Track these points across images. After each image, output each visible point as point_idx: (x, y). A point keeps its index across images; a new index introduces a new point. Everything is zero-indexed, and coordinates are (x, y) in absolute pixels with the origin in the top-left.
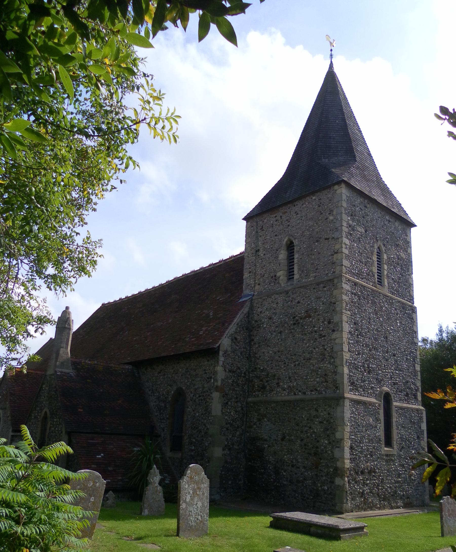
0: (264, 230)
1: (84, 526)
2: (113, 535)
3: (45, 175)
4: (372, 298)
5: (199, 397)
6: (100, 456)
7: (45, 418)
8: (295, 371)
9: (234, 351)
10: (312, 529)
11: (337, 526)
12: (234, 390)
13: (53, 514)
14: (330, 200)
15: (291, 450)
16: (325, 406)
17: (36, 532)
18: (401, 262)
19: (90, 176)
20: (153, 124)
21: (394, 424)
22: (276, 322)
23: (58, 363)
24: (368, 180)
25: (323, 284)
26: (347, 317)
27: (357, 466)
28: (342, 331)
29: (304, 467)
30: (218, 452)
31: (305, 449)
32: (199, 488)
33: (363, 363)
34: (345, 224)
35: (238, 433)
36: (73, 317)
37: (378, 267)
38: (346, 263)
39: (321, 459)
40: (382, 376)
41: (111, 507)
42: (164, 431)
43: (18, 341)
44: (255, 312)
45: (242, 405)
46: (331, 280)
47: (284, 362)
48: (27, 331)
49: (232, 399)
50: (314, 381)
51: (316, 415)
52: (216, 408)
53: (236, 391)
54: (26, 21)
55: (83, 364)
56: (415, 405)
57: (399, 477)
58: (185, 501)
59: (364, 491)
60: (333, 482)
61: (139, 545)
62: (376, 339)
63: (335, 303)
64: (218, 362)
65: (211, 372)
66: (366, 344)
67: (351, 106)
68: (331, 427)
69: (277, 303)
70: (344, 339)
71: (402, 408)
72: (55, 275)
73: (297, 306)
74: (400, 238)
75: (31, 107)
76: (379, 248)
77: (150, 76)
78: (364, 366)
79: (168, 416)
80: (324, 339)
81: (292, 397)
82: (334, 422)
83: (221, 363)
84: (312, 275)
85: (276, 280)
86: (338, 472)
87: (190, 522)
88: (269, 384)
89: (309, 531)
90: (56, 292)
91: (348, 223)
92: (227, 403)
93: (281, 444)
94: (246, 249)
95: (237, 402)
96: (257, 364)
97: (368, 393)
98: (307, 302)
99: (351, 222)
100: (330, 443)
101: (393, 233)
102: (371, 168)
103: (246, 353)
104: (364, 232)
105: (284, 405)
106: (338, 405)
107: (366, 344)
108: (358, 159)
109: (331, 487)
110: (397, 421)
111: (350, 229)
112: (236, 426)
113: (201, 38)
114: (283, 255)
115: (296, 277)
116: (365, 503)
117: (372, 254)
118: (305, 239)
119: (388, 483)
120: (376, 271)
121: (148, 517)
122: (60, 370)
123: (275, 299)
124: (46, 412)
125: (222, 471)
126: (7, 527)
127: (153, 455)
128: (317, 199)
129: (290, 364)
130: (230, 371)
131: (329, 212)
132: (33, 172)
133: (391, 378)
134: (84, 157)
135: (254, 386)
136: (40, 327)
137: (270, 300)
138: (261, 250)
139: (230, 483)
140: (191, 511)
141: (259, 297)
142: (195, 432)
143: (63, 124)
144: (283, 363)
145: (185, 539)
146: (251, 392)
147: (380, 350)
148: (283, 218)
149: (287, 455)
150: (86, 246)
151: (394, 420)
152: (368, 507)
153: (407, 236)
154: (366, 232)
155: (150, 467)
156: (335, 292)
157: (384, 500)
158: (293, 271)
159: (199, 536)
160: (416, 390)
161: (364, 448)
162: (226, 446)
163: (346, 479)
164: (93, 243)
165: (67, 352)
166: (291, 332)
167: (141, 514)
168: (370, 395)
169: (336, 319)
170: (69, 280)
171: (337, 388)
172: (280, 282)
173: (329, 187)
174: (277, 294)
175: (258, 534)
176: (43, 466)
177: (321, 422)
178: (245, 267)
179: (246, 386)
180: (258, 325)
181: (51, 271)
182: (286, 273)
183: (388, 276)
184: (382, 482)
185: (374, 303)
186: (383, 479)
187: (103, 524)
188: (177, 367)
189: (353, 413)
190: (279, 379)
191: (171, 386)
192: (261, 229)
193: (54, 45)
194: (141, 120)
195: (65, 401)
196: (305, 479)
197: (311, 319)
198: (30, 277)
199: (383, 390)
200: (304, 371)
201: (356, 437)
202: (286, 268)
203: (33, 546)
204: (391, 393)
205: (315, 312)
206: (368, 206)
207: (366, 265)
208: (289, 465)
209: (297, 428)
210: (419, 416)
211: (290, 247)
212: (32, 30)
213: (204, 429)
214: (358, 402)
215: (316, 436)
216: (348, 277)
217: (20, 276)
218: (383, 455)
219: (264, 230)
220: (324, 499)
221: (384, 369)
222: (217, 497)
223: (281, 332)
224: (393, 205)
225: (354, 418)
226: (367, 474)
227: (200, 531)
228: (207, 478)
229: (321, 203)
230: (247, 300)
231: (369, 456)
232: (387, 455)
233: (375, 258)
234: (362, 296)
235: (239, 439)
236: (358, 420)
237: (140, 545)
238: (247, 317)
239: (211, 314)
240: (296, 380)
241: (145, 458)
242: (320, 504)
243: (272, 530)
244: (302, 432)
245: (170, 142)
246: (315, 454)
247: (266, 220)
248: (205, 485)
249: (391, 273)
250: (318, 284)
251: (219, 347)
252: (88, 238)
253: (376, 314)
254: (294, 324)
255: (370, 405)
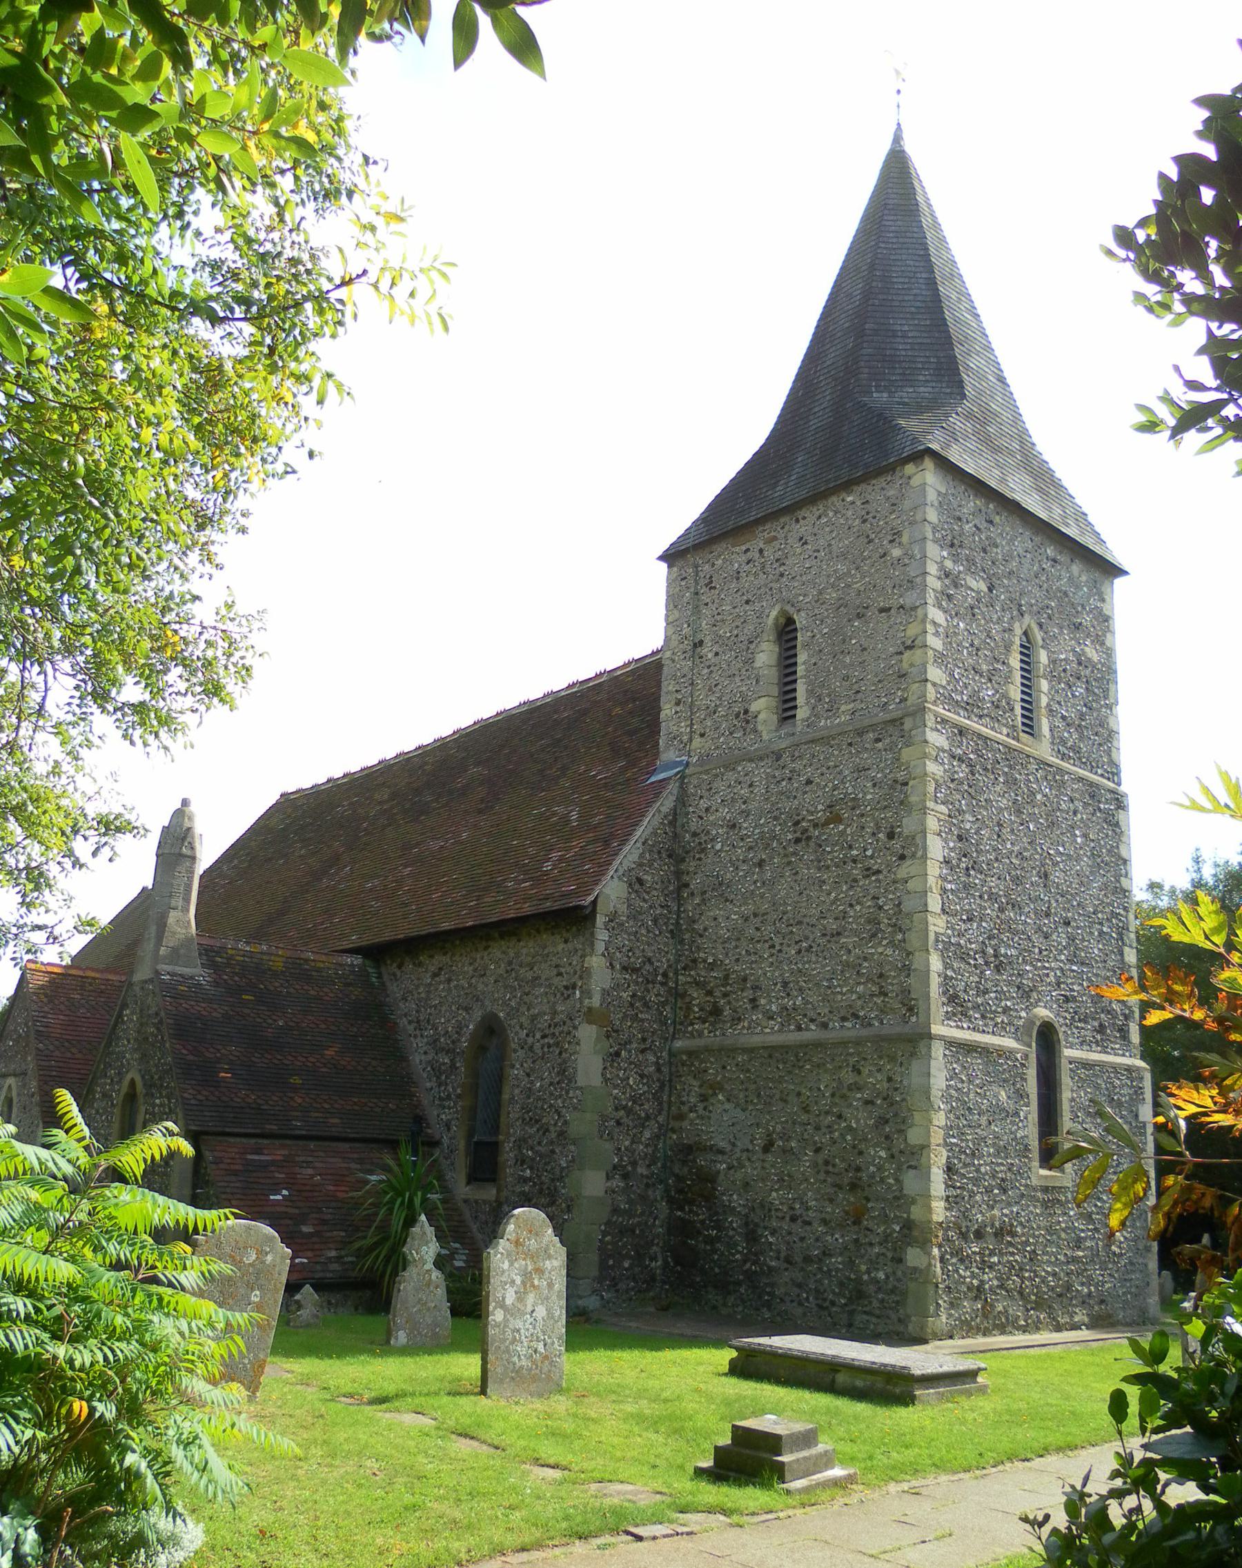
0: (715, 588)
1: (231, 1355)
2: (312, 1394)
3: (109, 425)
4: (1006, 770)
5: (544, 1037)
6: (279, 1197)
7: (131, 1097)
8: (800, 966)
9: (634, 916)
10: (841, 1378)
11: (904, 1368)
12: (635, 1018)
13: (151, 1321)
14: (893, 505)
15: (789, 1176)
16: (881, 1058)
17: (106, 1358)
18: (1088, 672)
19: (224, 427)
20: (384, 285)
21: (1066, 1107)
22: (749, 837)
23: (163, 951)
24: (996, 450)
25: (874, 731)
26: (939, 820)
27: (966, 1218)
28: (925, 857)
29: (825, 1222)
30: (593, 1184)
31: (827, 1172)
32: (540, 1271)
33: (983, 942)
34: (932, 569)
35: (647, 1134)
36: (200, 827)
37: (1023, 684)
38: (935, 674)
39: (868, 1200)
40: (1032, 980)
41: (308, 1326)
42: (449, 1129)
43: (47, 879)
44: (691, 809)
45: (658, 1058)
46: (897, 722)
47: (770, 943)
48: (70, 854)
49: (630, 1042)
50: (851, 991)
51: (856, 1083)
52: (589, 1063)
53: (642, 1020)
54: (35, 23)
55: (230, 952)
56: (1123, 1055)
57: (1079, 1248)
58: (502, 1305)
59: (982, 1282)
60: (900, 1261)
61: (380, 1414)
62: (1017, 880)
63: (906, 784)
64: (592, 944)
65: (575, 973)
66: (991, 894)
67: (951, 246)
68: (896, 1115)
69: (751, 786)
70: (931, 880)
71: (1087, 1065)
72: (142, 703)
73: (806, 793)
74: (1083, 607)
75: (68, 245)
76: (1025, 633)
77: (381, 163)
78: (983, 952)
79: (459, 1091)
80: (878, 881)
81: (793, 1037)
82: (903, 1100)
83: (600, 947)
84: (843, 708)
85: (748, 722)
86: (914, 1233)
87: (516, 1359)
88: (729, 1003)
89: (833, 1381)
90: (148, 749)
91: (942, 567)
92: (618, 1054)
93: (763, 1161)
94: (667, 639)
95: (643, 1051)
96: (699, 948)
97: (996, 1025)
98: (830, 781)
99: (949, 564)
100: (893, 1156)
101: (1065, 594)
102: (1006, 415)
103: (669, 919)
104: (986, 589)
105: (770, 1056)
106: (913, 1054)
107: (991, 894)
108: (969, 390)
109: (894, 1273)
110: (1073, 1100)
111: (947, 582)
112: (643, 1115)
113: (458, 62)
114: (766, 656)
115: (802, 713)
116: (985, 1316)
117: (1008, 648)
118: (827, 610)
119: (1049, 1263)
120: (1019, 696)
121: (404, 1351)
122: (169, 968)
123: (746, 775)
124: (133, 1082)
125: (604, 1234)
126: (30, 1345)
127: (419, 1194)
128: (858, 503)
129: (785, 948)
130: (625, 968)
131: (890, 538)
132: (80, 418)
133: (1058, 984)
134: (215, 385)
135: (689, 1008)
136: (105, 844)
137: (731, 776)
138: (707, 640)
139: (626, 1265)
140: (518, 1331)
141: (701, 769)
142: (533, 1131)
143: (151, 291)
144: (767, 945)
145: (503, 1403)
146: (681, 1023)
147: (1027, 909)
148: (766, 554)
149: (776, 1190)
150: (224, 628)
151: (1066, 1095)
152: (996, 1326)
153: (1103, 600)
154: (990, 590)
155: (411, 1221)
156: (906, 754)
157: (1038, 1306)
158: (795, 698)
159: (540, 1396)
160: (1126, 1017)
161: (983, 1169)
162: (615, 1167)
163: (936, 1251)
164: (244, 621)
165: (185, 920)
166: (789, 863)
167: (388, 1342)
168: (998, 1029)
169: (908, 825)
170: (179, 720)
171: (911, 1009)
172: (760, 728)
173: (891, 469)
174: (751, 760)
175: (698, 1390)
176: (119, 1193)
177: (868, 1102)
178: (664, 689)
179: (668, 1008)
180: (700, 843)
181: (131, 692)
182: (774, 704)
183: (1051, 711)
184: (1031, 1259)
185: (1011, 782)
186: (1034, 1251)
187: (288, 1366)
188: (482, 958)
189: (953, 1075)
190: (755, 988)
191: (467, 1009)
192: (706, 585)
193: (104, 82)
194: (354, 276)
195: (185, 1052)
196: (826, 1253)
197: (841, 827)
198: (78, 711)
199: (1035, 1016)
200: (824, 966)
201: (962, 1140)
202: (775, 691)
203: (98, 1395)
204: (1056, 1025)
205: (853, 809)
206: (997, 519)
207: (990, 680)
208: (783, 1218)
209: (804, 1117)
210: (1132, 1087)
211: (786, 632)
212: (50, 45)
213: (556, 1124)
214: (969, 1048)
215: (854, 1140)
216: (943, 711)
217: (49, 706)
218: (1034, 1189)
219: (715, 588)
220: (875, 1304)
221: (1039, 960)
222: (592, 1303)
223: (761, 864)
224: (1064, 517)
225: (958, 1090)
226: (991, 1239)
227: (543, 1381)
228: (559, 1245)
229: (868, 513)
230: (669, 778)
231: (996, 1191)
232: (1046, 1190)
233: (1015, 661)
234: (979, 762)
235: (650, 1150)
236: (967, 1094)
237: (382, 1415)
238: (670, 823)
239: (574, 816)
240: (801, 990)
241: (399, 1200)
242: (866, 1317)
243: (733, 1381)
244: (817, 1128)
245: (432, 331)
246: (854, 1187)
247: (720, 561)
248: (556, 1263)
249: (1059, 703)
250: (861, 733)
251: (594, 902)
252: (229, 606)
253: (1019, 812)
254: (798, 841)
255: (1000, 1056)
